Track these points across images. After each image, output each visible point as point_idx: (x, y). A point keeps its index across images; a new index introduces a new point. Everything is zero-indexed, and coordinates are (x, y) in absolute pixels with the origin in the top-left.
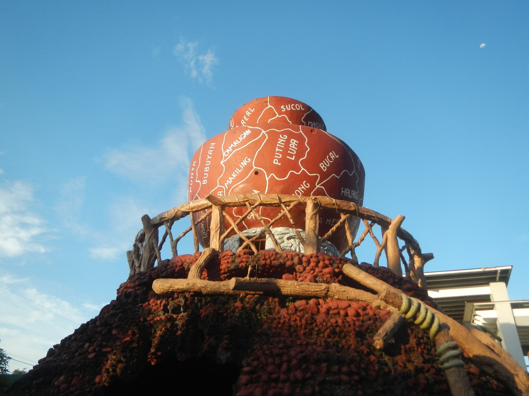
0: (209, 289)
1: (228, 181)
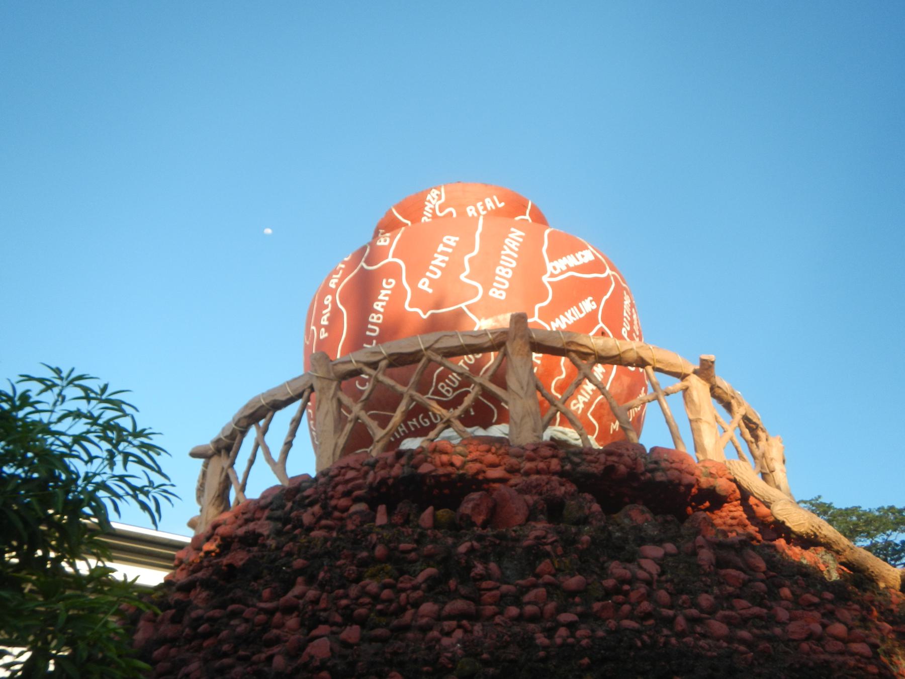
0: (856, 556)
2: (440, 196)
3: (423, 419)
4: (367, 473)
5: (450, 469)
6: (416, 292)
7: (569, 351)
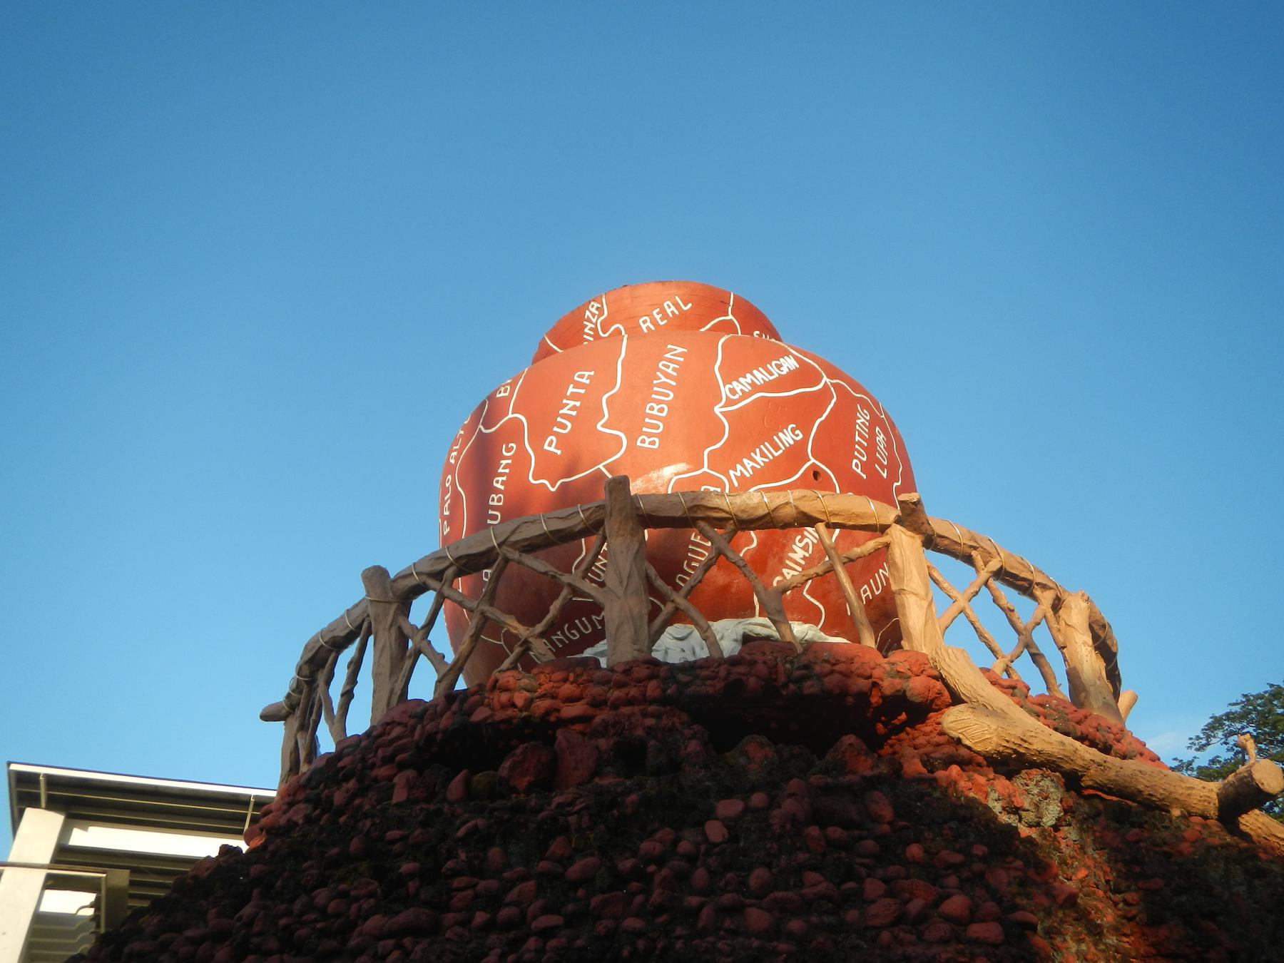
0: (1112, 774)
1: (739, 467)
2: (600, 310)
3: (569, 630)
4: (414, 728)
5: (510, 712)
6: (542, 455)
7: (695, 520)
